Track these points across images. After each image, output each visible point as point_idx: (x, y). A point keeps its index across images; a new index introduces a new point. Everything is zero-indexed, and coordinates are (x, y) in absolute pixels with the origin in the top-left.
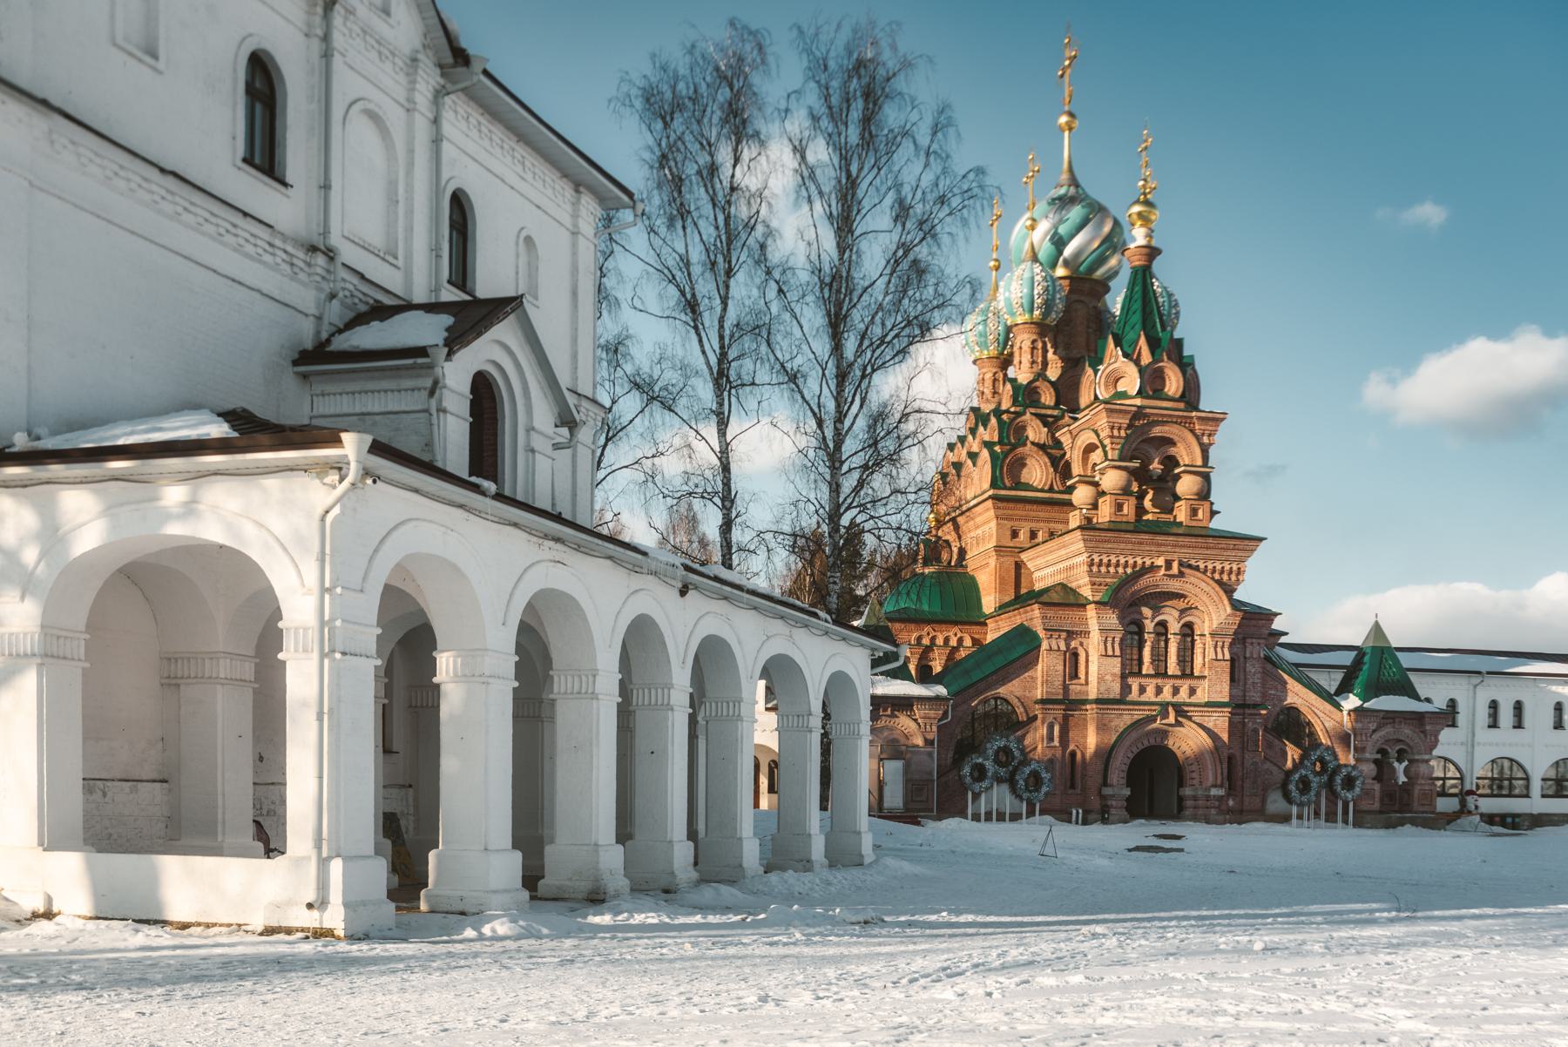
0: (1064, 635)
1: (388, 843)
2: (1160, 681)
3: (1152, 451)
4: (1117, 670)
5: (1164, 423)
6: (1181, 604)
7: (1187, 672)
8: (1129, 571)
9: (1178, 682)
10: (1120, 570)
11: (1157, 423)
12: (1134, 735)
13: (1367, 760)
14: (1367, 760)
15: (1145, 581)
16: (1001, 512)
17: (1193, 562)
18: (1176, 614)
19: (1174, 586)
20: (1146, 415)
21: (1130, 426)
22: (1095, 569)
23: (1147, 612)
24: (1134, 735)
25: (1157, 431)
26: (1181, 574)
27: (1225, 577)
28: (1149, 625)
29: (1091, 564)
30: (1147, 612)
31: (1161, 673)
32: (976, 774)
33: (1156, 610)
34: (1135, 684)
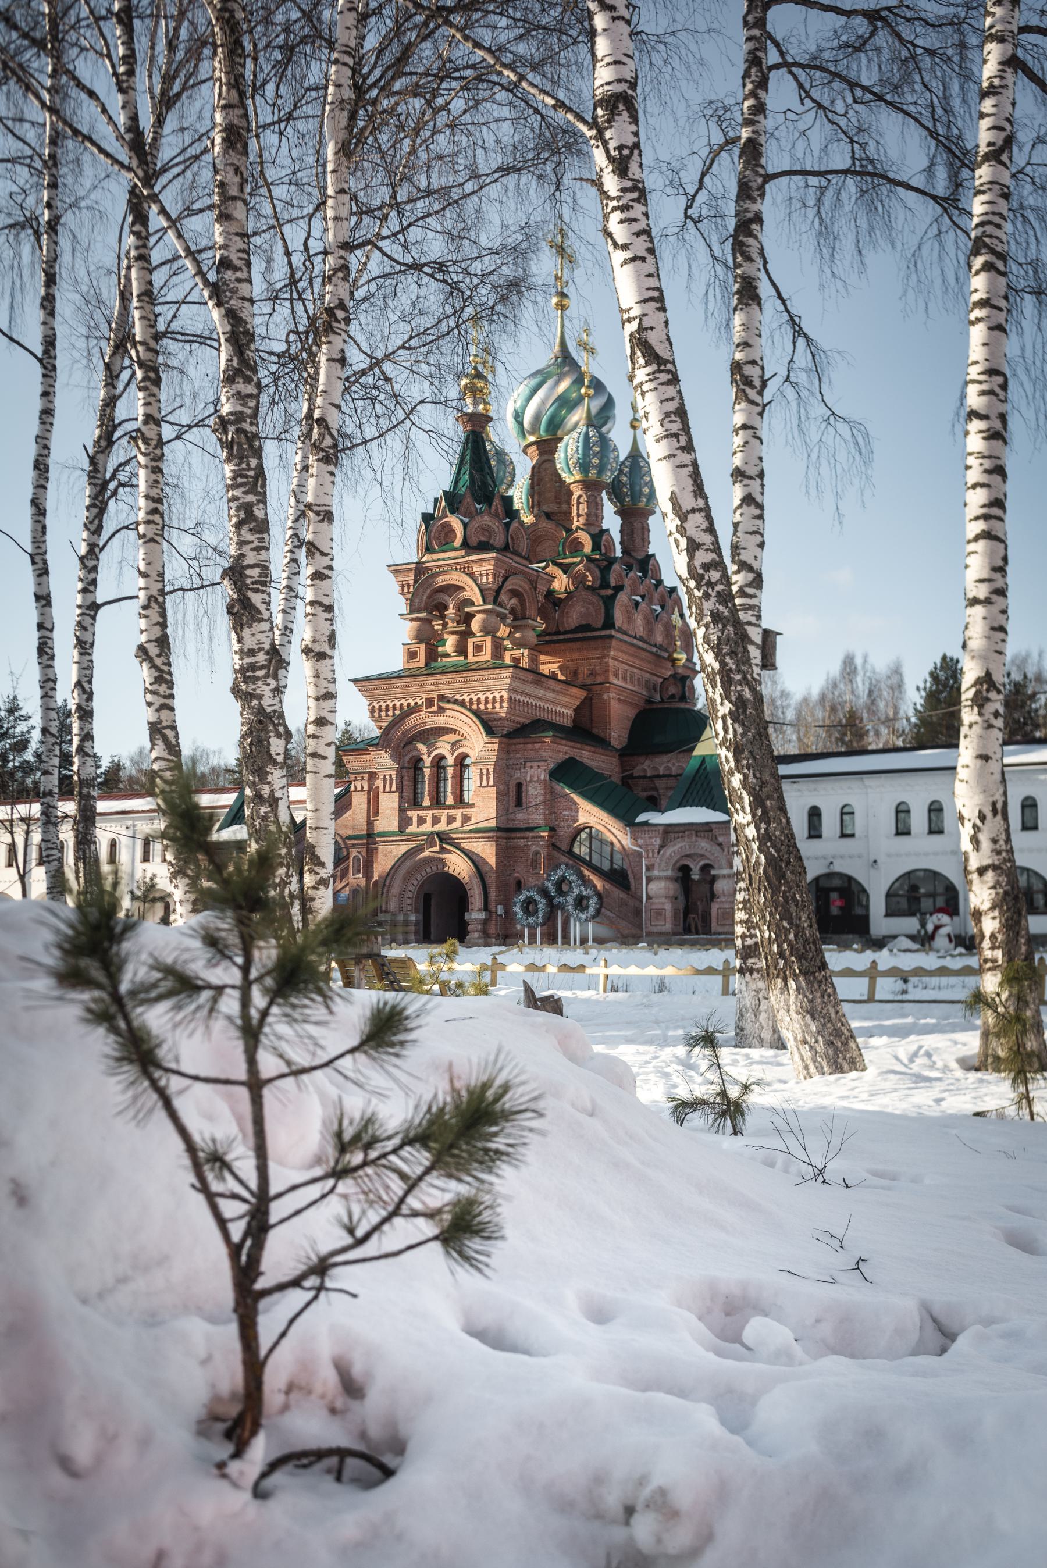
0: (366, 776)
1: (608, 945)
2: (436, 812)
3: (446, 598)
4: (396, 805)
5: (444, 573)
6: (452, 737)
7: (460, 801)
8: (397, 712)
9: (452, 812)
10: (390, 713)
11: (437, 574)
12: (408, 864)
13: (659, 878)
14: (659, 878)
15: (412, 721)
16: (517, 684)
17: (458, 697)
18: (449, 747)
19: (440, 721)
20: (428, 569)
21: (416, 581)
22: (376, 714)
23: (422, 747)
24: (408, 864)
25: (441, 581)
26: (441, 710)
27: (482, 707)
28: (427, 761)
29: (373, 711)
30: (422, 747)
31: (438, 802)
32: (585, 902)
33: (431, 747)
34: (414, 815)
